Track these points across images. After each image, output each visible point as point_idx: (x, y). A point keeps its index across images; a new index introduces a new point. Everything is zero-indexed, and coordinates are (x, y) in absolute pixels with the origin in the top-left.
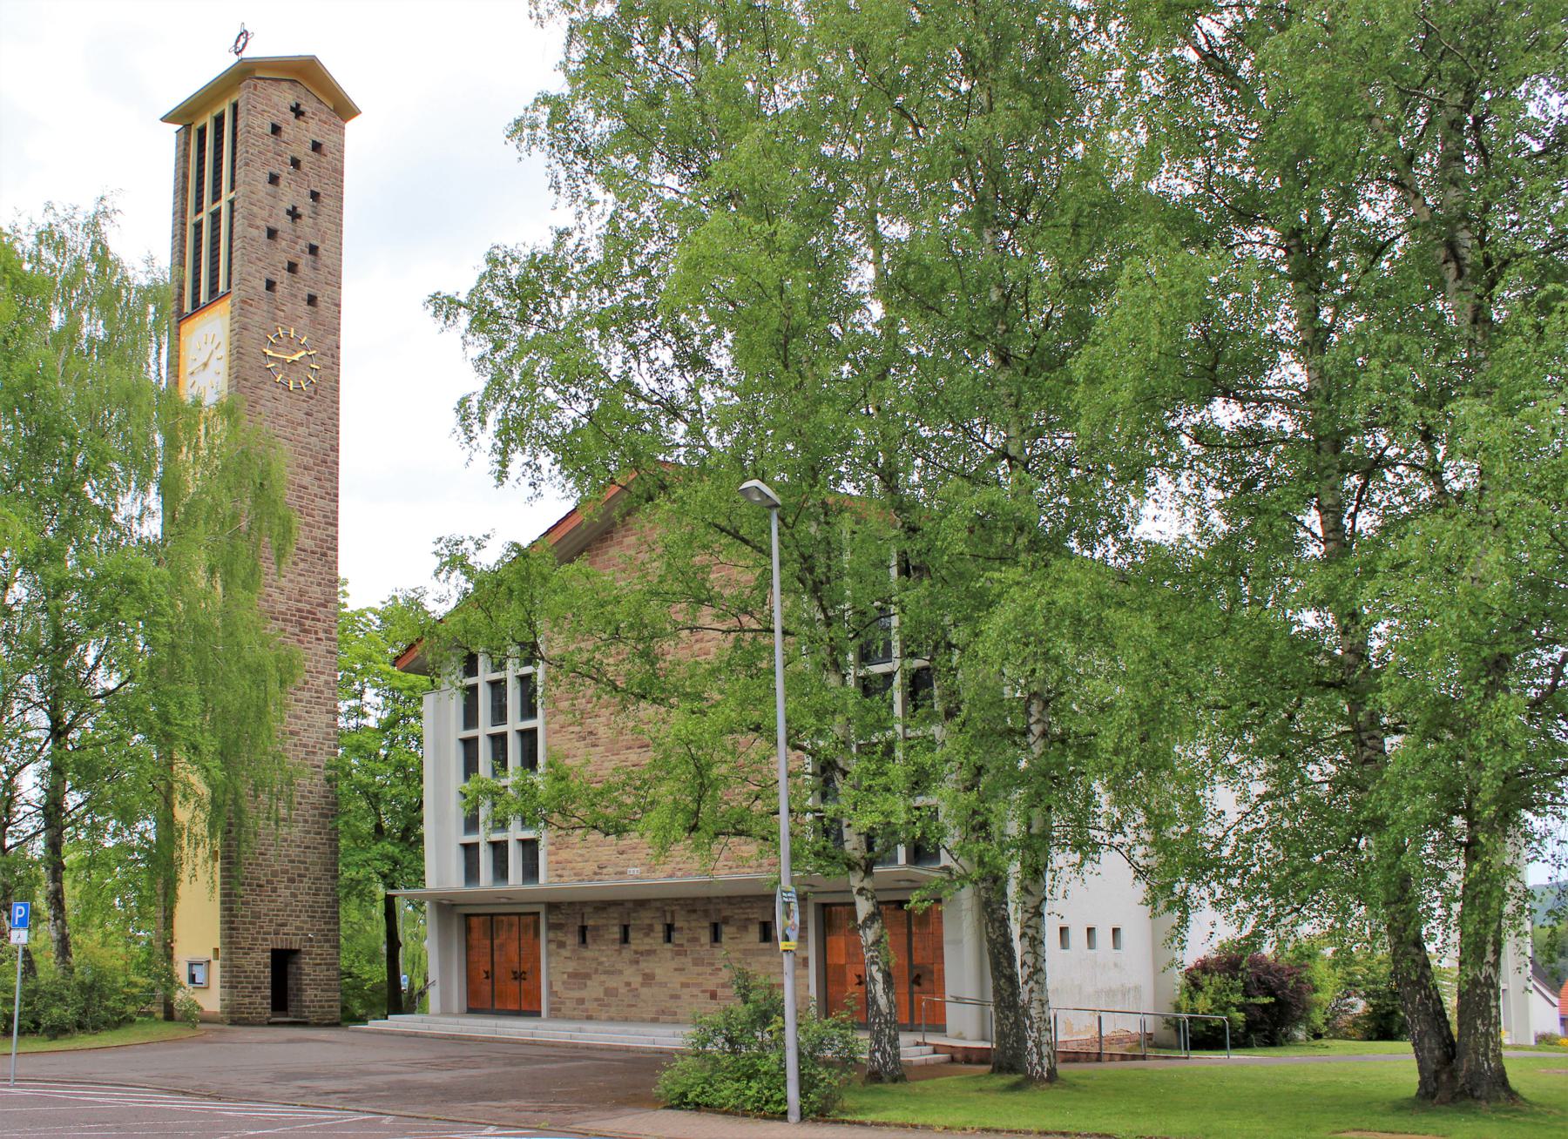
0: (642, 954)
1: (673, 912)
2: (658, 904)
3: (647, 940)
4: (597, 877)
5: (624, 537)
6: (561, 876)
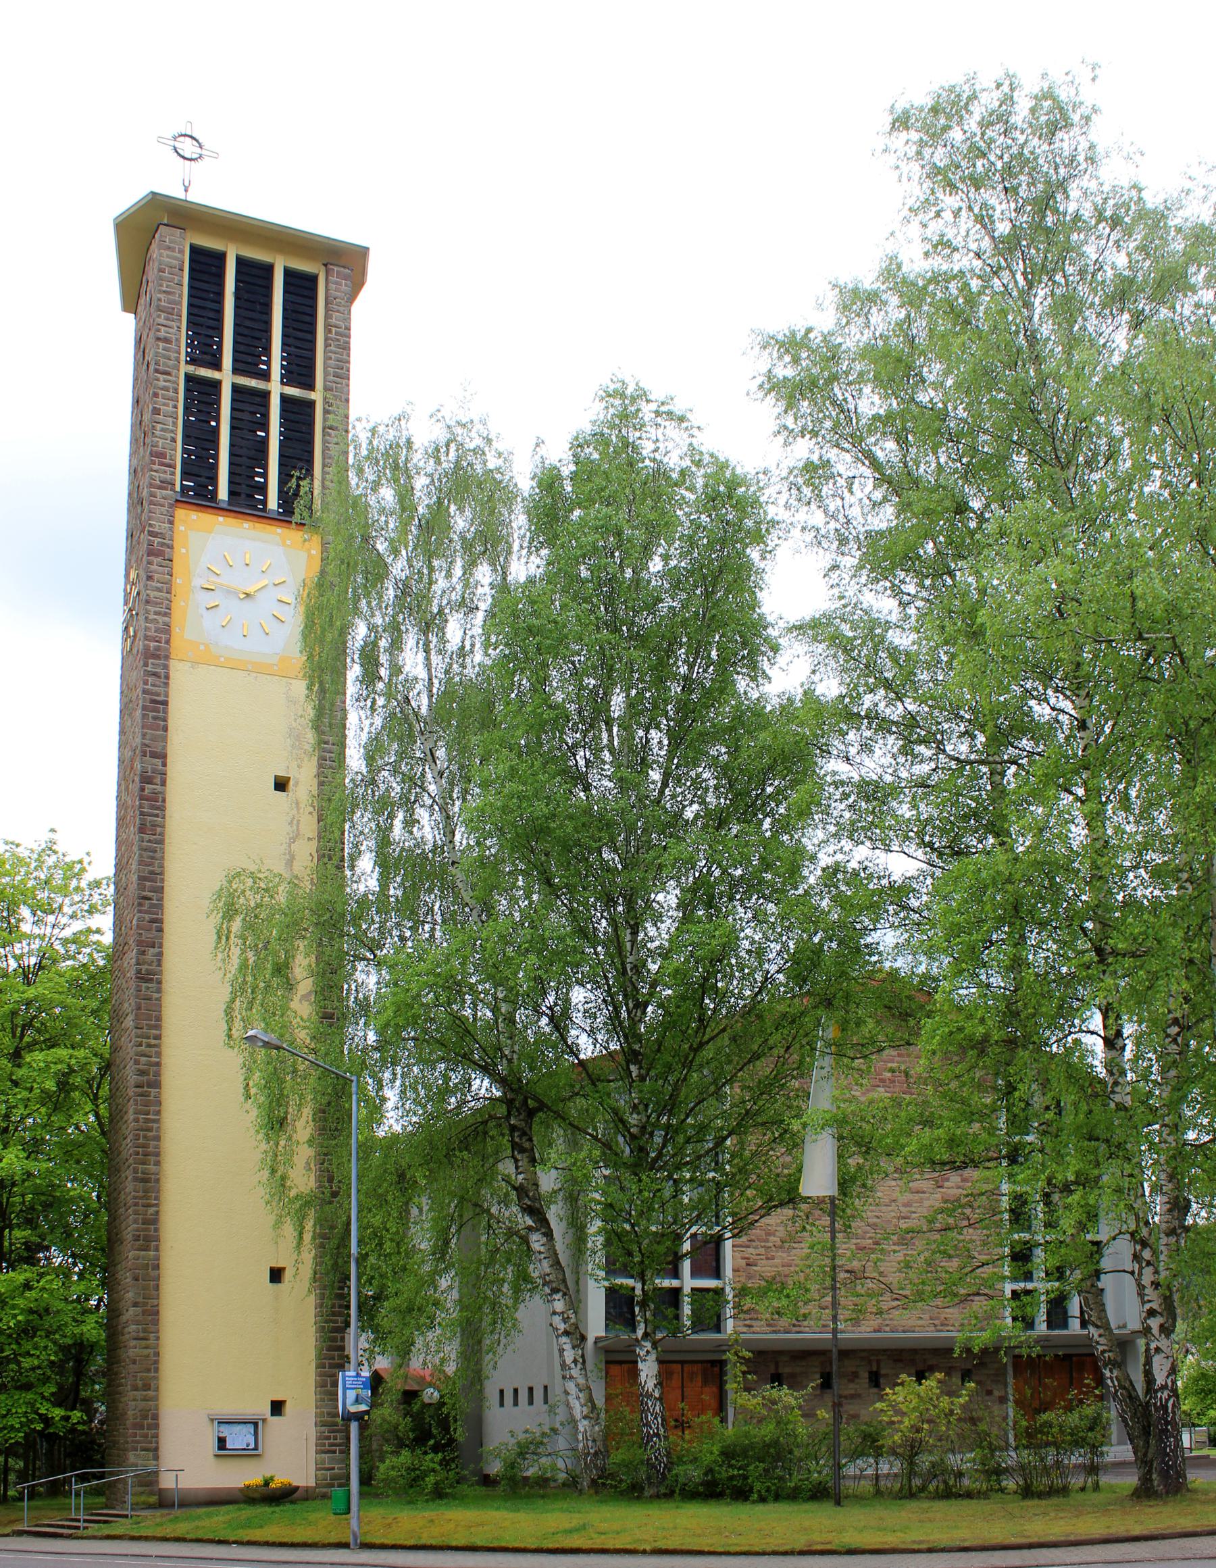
0: (846, 1397)
1: (878, 1362)
2: (863, 1354)
3: (851, 1386)
4: (797, 1329)
5: (879, 394)
6: (750, 1326)
